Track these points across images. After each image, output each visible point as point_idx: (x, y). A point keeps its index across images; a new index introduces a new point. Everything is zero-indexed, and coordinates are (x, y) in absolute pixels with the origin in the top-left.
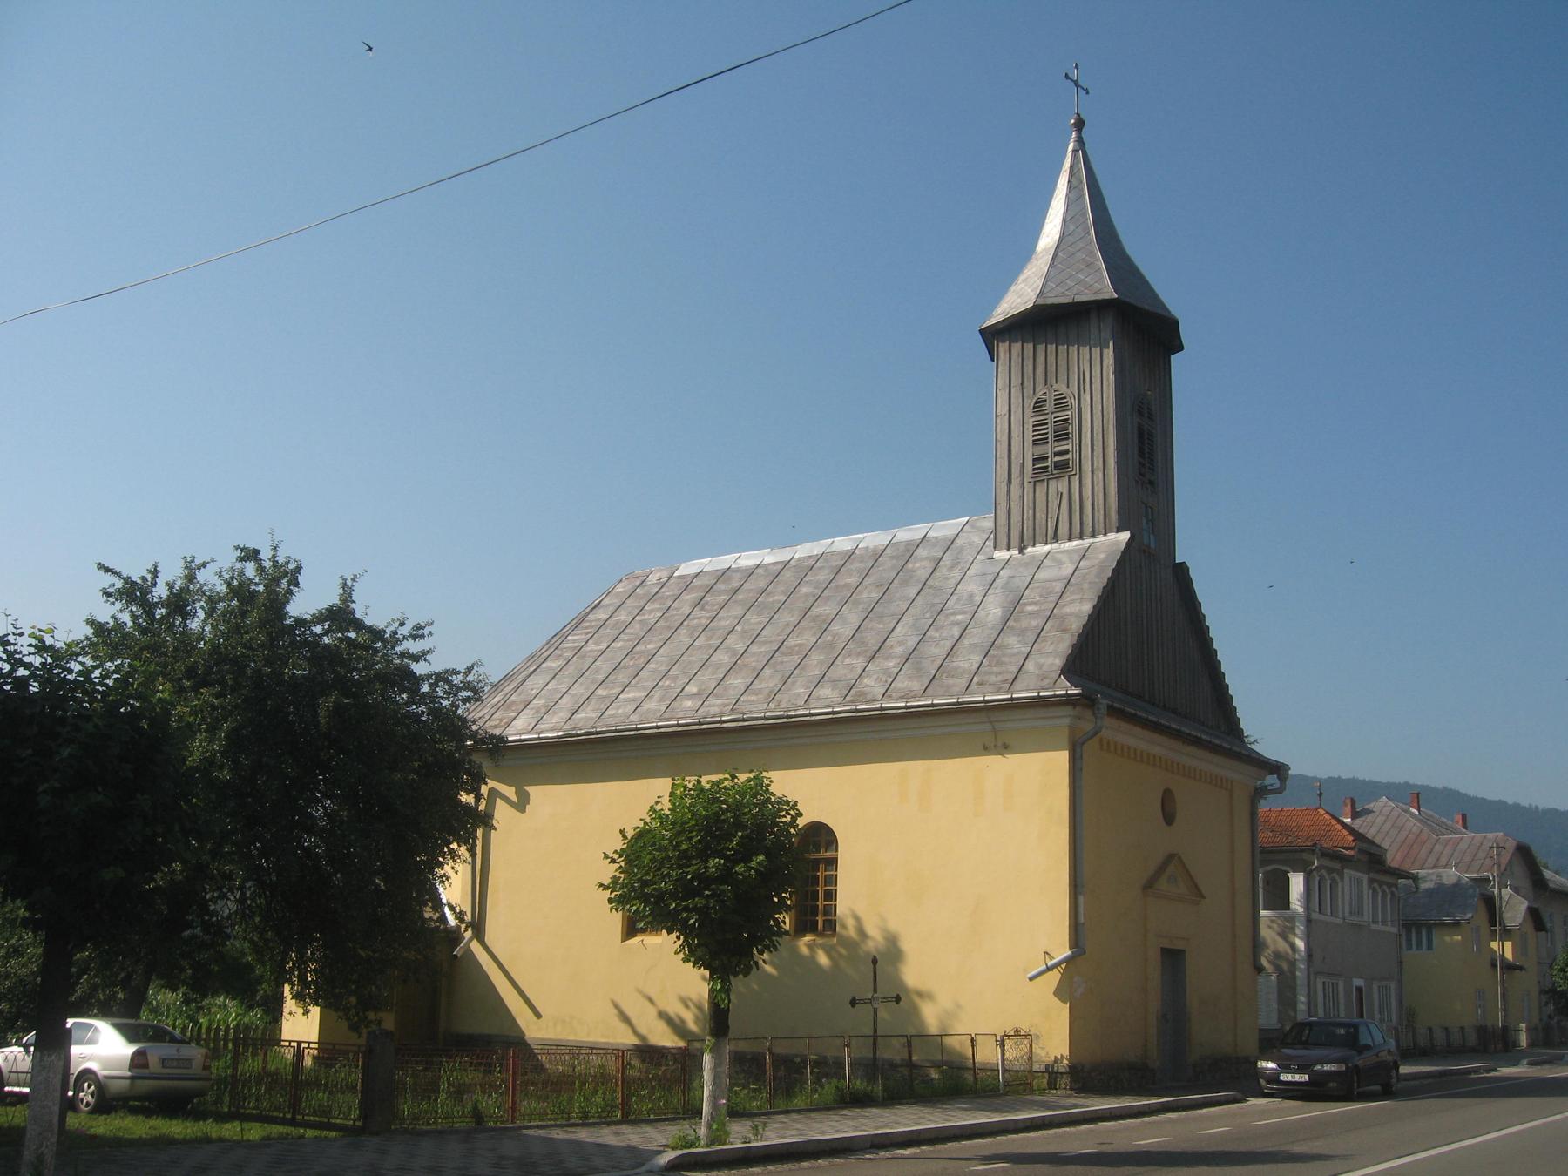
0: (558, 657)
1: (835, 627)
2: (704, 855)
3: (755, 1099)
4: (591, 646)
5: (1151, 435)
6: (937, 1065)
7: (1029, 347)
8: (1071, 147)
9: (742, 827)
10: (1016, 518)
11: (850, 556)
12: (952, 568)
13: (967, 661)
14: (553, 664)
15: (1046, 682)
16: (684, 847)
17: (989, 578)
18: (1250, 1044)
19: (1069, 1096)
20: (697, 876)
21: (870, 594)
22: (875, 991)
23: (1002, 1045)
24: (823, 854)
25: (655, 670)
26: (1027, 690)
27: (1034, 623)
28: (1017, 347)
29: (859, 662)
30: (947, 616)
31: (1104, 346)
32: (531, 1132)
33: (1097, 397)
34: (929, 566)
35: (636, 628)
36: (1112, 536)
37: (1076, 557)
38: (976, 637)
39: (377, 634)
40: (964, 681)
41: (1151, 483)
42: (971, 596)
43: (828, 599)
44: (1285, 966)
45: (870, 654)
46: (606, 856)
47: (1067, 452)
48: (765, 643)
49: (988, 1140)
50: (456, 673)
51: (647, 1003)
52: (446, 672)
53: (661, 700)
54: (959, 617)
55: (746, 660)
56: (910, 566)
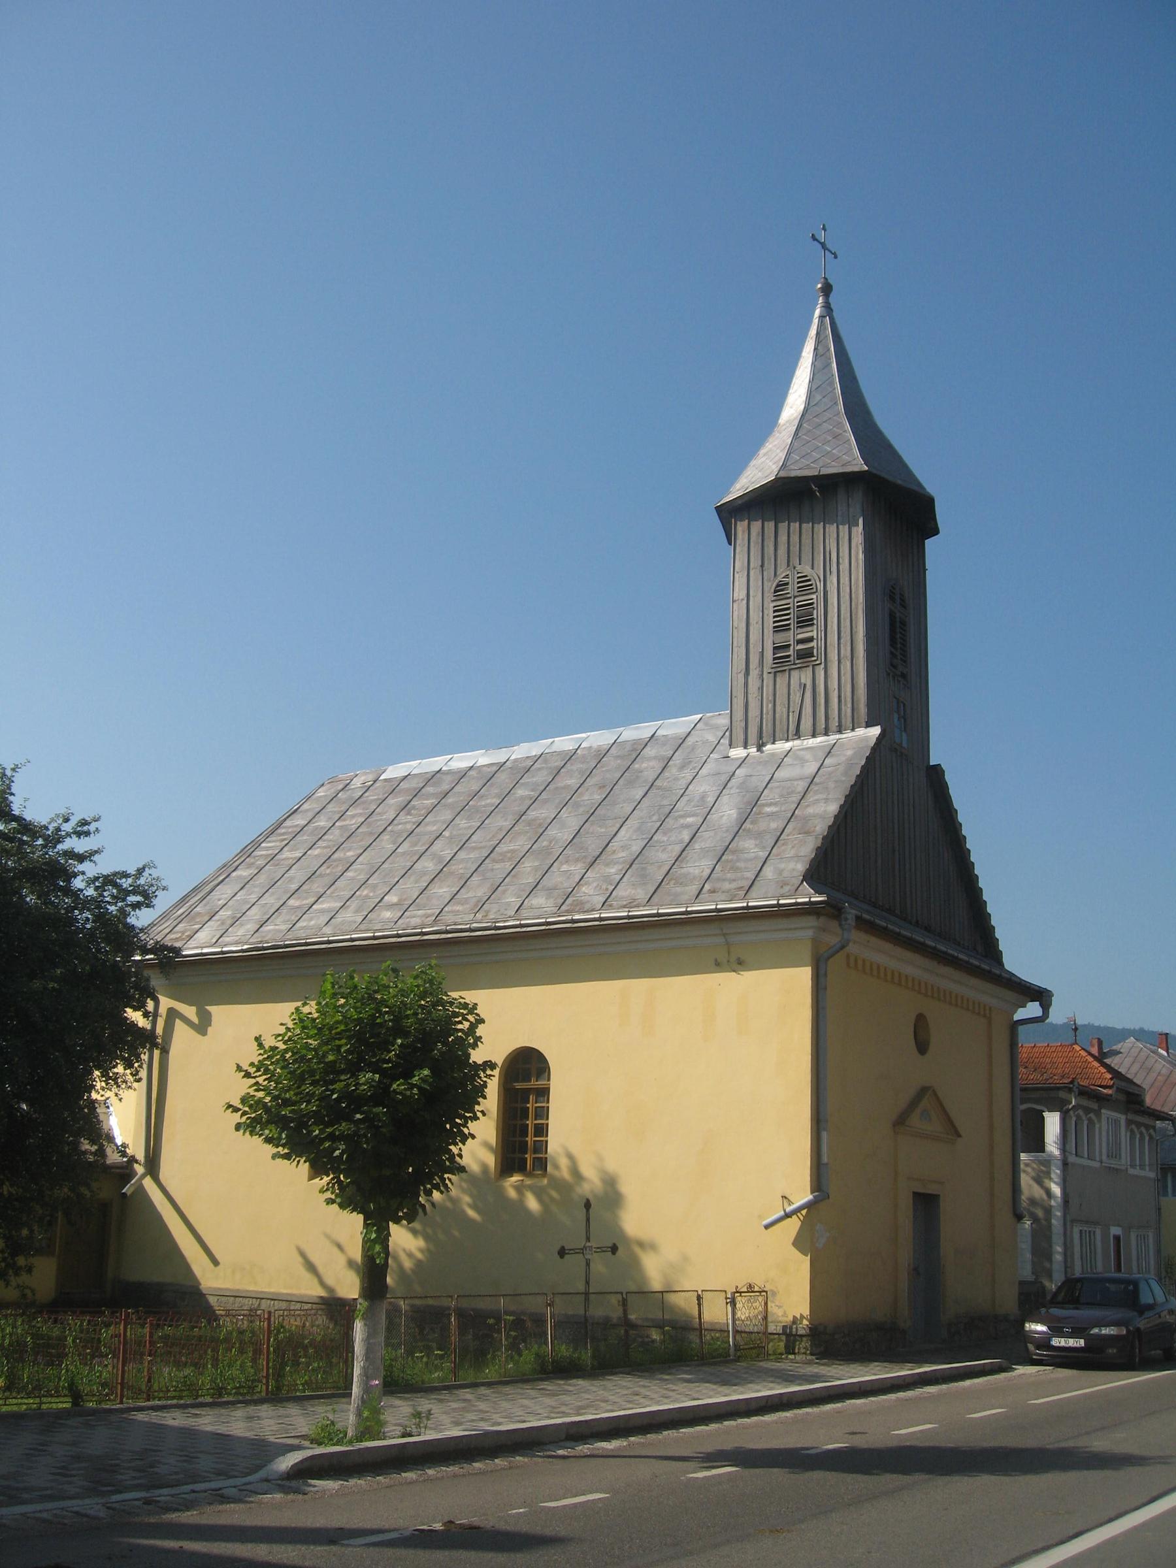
0: (250, 866)
1: (552, 832)
2: (354, 1069)
3: (437, 1368)
4: (286, 854)
5: (903, 623)
6: (660, 1325)
7: (770, 526)
8: (817, 312)
9: (404, 1034)
10: (754, 712)
11: (571, 756)
12: (682, 767)
13: (698, 866)
14: (244, 872)
15: (787, 888)
16: (331, 1058)
17: (724, 778)
18: (1009, 1302)
19: (810, 1363)
20: (346, 1095)
21: (591, 796)
22: (588, 1239)
23: (733, 1303)
24: (534, 1083)
25: (353, 879)
26: (766, 898)
27: (773, 825)
28: (756, 526)
29: (577, 869)
30: (676, 819)
31: (852, 524)
32: (140, 1416)
33: (845, 580)
34: (658, 766)
35: (335, 836)
36: (861, 732)
37: (822, 755)
38: (709, 840)
39: (26, 827)
40: (693, 889)
41: (903, 676)
42: (703, 798)
43: (546, 801)
44: (1040, 1213)
45: (590, 859)
46: (239, 1068)
47: (811, 639)
48: (474, 848)
49: (713, 1426)
50: (125, 875)
51: (336, 1250)
52: (115, 874)
53: (357, 911)
54: (690, 820)
55: (453, 867)
56: (636, 766)
